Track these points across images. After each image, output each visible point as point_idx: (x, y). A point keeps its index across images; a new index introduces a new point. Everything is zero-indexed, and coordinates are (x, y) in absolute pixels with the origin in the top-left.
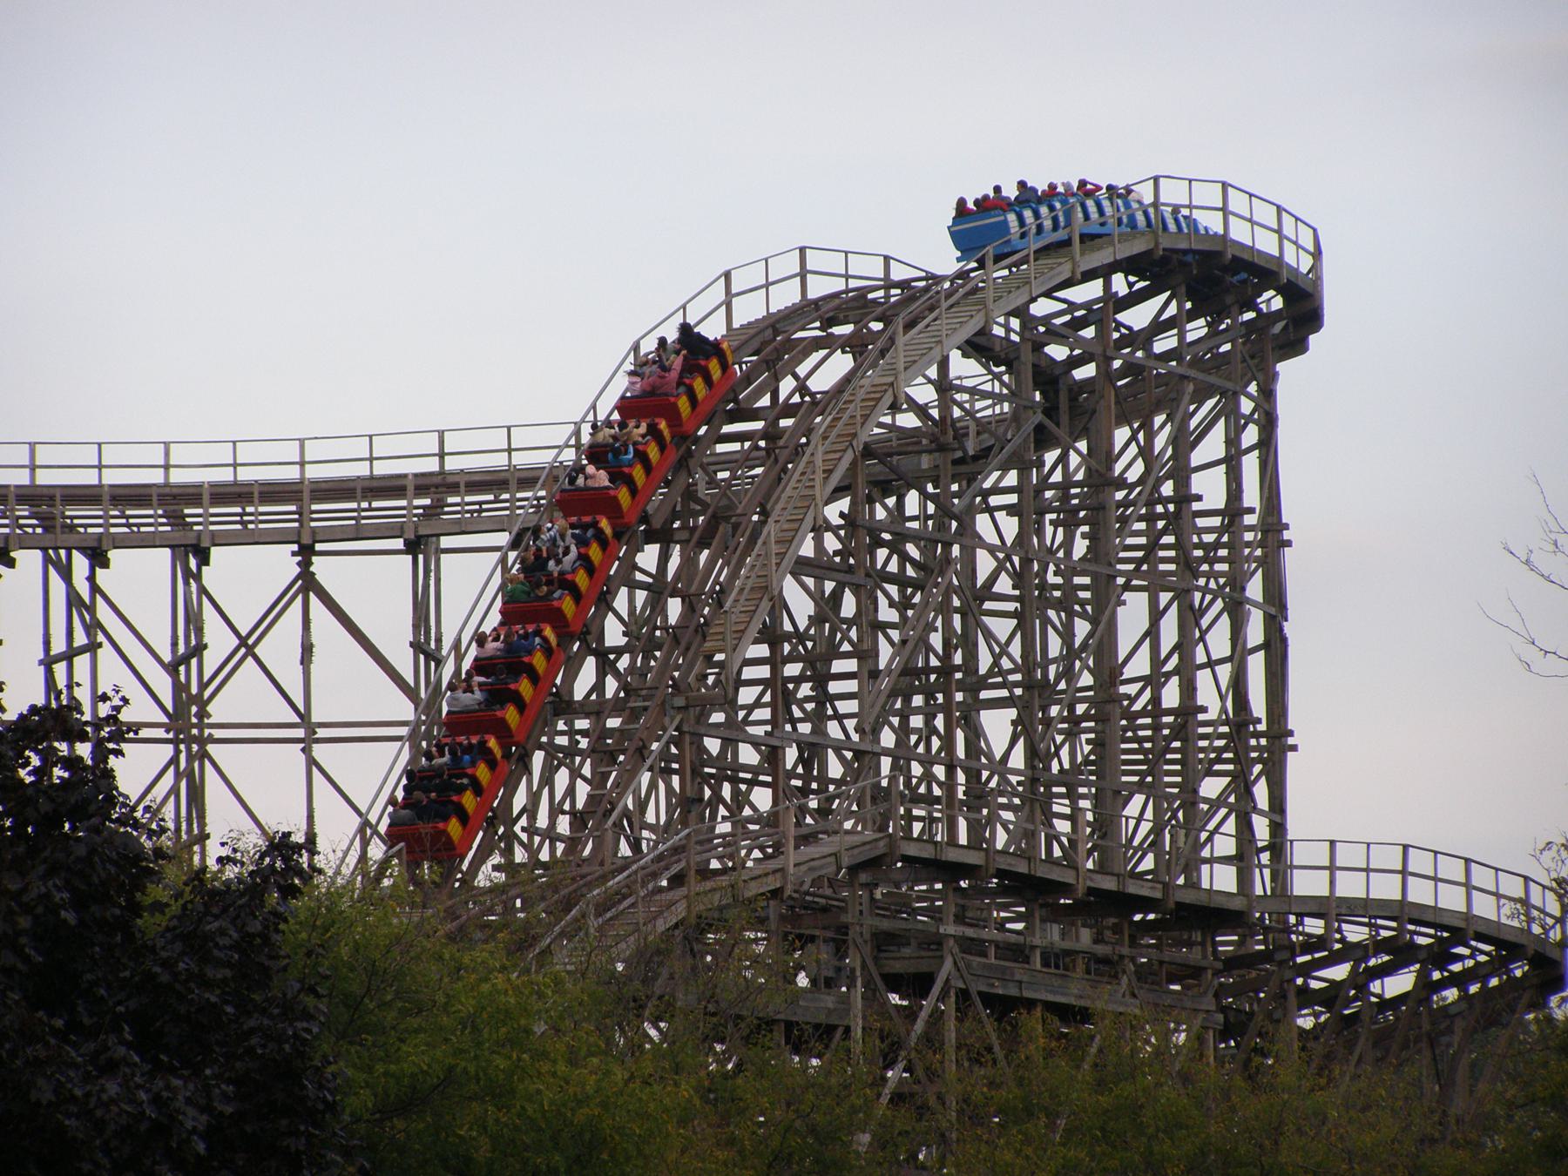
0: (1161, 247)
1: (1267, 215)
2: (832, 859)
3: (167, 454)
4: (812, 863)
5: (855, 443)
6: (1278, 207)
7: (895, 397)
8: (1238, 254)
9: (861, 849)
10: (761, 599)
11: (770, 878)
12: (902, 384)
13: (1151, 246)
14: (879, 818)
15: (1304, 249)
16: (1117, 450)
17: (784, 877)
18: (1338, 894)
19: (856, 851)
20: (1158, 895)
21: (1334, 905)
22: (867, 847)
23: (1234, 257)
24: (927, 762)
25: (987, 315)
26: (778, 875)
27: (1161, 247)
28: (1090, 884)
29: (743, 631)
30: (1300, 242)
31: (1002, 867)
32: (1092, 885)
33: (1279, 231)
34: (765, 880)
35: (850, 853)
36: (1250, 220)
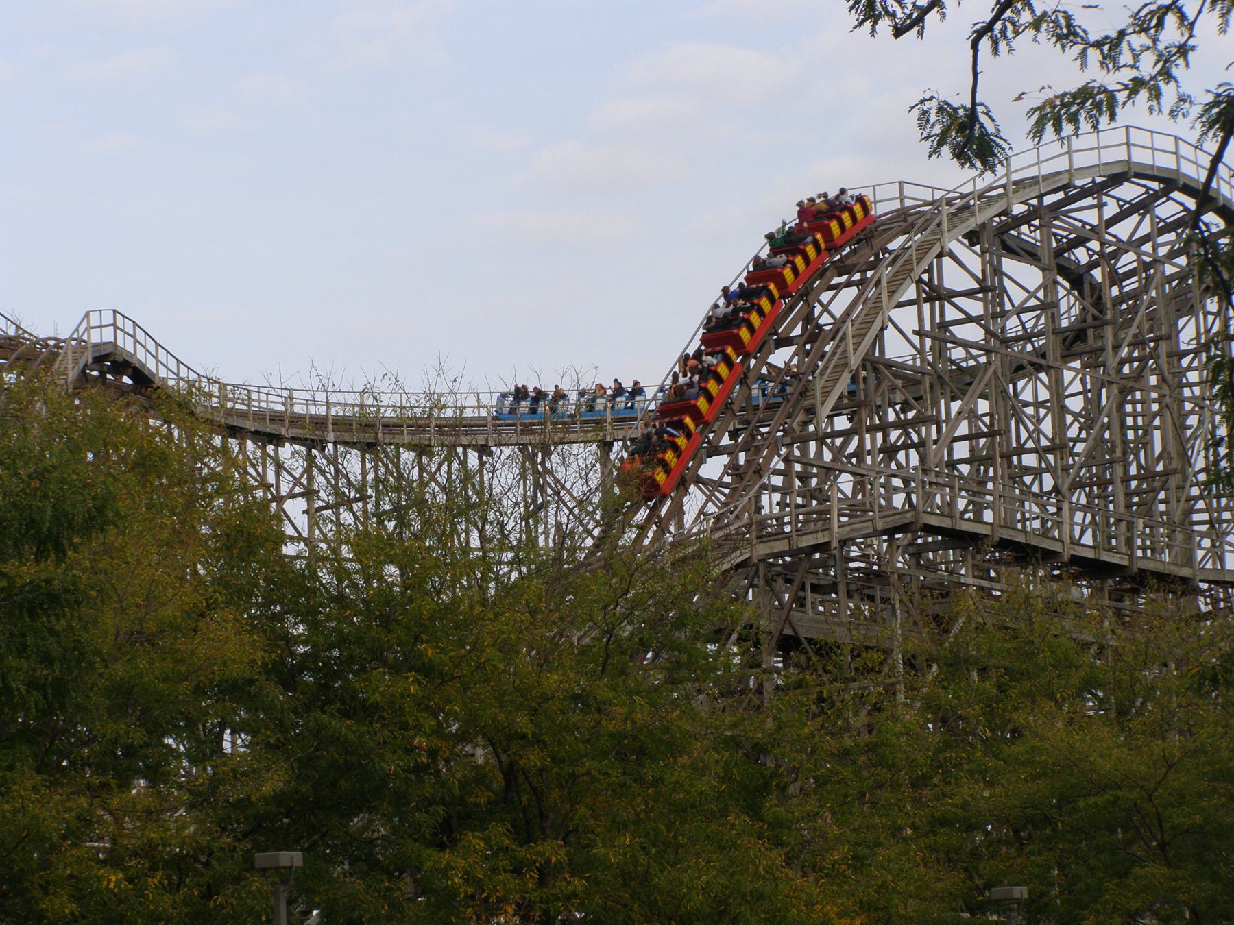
1: (1169, 144)
2: (869, 524)
3: (478, 400)
4: (854, 526)
5: (912, 274)
6: (1176, 137)
7: (942, 248)
8: (1187, 182)
9: (891, 518)
10: (843, 371)
14: (714, 320)
15: (1191, 162)
17: (831, 535)
19: (888, 519)
20: (1126, 563)
22: (897, 517)
25: (1008, 201)
27: (1133, 170)
28: (1072, 552)
29: (829, 392)
30: (1199, 162)
32: (1075, 553)
33: (1176, 153)
34: (815, 535)
35: (884, 520)
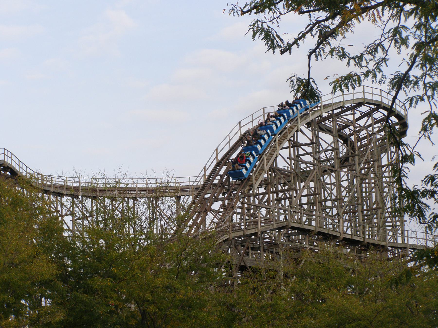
0: (365, 101)
2: (272, 226)
5: (287, 138)
6: (381, 90)
7: (298, 128)
8: (385, 106)
11: (254, 230)
12: (299, 125)
13: (363, 101)
16: (382, 157)
17: (258, 230)
18: (410, 243)
19: (278, 224)
20: (362, 240)
21: (409, 245)
23: (398, 114)
24: (369, 235)
25: (321, 112)
26: (256, 229)
27: (365, 101)
28: (344, 236)
31: (320, 231)
36: (388, 99)
